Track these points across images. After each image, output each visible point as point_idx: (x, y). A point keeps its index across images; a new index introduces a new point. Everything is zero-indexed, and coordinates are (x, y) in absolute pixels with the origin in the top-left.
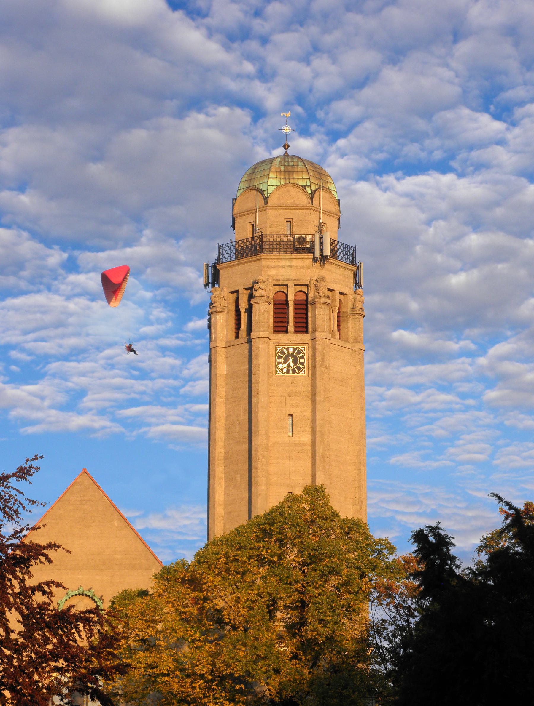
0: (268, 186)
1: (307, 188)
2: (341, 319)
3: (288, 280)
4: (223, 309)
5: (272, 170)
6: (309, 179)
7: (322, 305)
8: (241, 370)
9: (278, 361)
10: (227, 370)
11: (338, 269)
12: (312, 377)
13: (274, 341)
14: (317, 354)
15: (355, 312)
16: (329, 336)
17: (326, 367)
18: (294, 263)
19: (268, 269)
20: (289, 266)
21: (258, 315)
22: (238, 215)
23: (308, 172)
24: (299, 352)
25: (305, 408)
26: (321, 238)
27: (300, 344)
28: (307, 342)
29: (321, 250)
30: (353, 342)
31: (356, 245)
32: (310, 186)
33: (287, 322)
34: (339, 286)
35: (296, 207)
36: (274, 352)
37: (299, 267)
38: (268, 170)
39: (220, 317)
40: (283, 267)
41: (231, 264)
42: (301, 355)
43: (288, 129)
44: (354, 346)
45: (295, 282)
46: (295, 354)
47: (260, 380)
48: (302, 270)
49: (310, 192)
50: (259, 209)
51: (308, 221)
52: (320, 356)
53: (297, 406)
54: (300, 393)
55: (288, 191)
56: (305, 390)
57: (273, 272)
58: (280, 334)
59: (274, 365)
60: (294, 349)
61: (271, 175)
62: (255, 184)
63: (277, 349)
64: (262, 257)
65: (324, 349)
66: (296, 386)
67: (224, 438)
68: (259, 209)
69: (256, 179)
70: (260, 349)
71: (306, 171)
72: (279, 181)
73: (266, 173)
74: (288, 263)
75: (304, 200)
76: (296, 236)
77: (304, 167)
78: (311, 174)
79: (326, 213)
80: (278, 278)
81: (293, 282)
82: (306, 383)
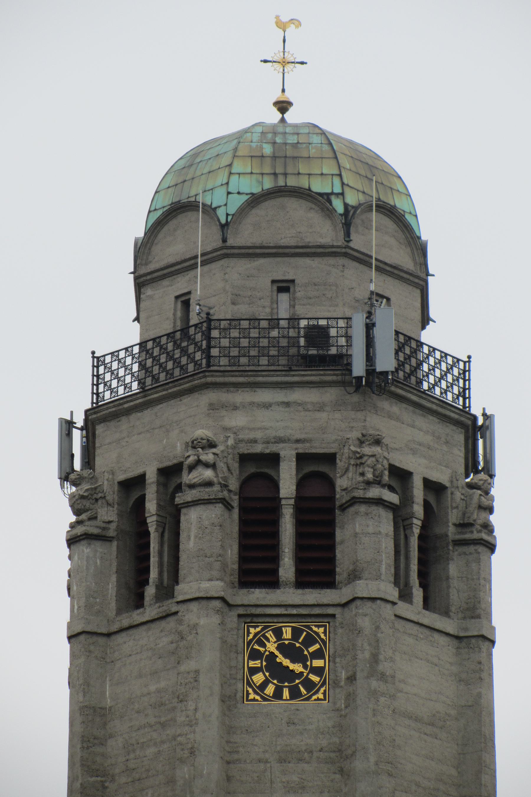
0: (229, 193)
1: (333, 198)
3: (280, 440)
4: (104, 529)
8: (149, 694)
9: (252, 664)
13: (241, 611)
15: (468, 536)
16: (393, 593)
17: (383, 677)
19: (224, 413)
20: (283, 403)
22: (149, 277)
23: (336, 158)
24: (310, 640)
26: (370, 327)
27: (313, 620)
28: (330, 611)
29: (370, 358)
30: (464, 618)
31: (469, 357)
32: (342, 194)
33: (276, 559)
34: (423, 461)
36: (241, 641)
37: (309, 407)
40: (267, 406)
41: (126, 406)
42: (316, 647)
44: (466, 629)
45: (299, 445)
46: (298, 645)
48: (318, 415)
50: (205, 258)
51: (337, 286)
54: (311, 752)
58: (257, 591)
59: (240, 676)
60: (296, 633)
62: (193, 193)
65: (378, 628)
67: (113, 526)
68: (205, 258)
71: (331, 155)
72: (258, 181)
74: (279, 396)
76: (303, 323)
79: (388, 268)
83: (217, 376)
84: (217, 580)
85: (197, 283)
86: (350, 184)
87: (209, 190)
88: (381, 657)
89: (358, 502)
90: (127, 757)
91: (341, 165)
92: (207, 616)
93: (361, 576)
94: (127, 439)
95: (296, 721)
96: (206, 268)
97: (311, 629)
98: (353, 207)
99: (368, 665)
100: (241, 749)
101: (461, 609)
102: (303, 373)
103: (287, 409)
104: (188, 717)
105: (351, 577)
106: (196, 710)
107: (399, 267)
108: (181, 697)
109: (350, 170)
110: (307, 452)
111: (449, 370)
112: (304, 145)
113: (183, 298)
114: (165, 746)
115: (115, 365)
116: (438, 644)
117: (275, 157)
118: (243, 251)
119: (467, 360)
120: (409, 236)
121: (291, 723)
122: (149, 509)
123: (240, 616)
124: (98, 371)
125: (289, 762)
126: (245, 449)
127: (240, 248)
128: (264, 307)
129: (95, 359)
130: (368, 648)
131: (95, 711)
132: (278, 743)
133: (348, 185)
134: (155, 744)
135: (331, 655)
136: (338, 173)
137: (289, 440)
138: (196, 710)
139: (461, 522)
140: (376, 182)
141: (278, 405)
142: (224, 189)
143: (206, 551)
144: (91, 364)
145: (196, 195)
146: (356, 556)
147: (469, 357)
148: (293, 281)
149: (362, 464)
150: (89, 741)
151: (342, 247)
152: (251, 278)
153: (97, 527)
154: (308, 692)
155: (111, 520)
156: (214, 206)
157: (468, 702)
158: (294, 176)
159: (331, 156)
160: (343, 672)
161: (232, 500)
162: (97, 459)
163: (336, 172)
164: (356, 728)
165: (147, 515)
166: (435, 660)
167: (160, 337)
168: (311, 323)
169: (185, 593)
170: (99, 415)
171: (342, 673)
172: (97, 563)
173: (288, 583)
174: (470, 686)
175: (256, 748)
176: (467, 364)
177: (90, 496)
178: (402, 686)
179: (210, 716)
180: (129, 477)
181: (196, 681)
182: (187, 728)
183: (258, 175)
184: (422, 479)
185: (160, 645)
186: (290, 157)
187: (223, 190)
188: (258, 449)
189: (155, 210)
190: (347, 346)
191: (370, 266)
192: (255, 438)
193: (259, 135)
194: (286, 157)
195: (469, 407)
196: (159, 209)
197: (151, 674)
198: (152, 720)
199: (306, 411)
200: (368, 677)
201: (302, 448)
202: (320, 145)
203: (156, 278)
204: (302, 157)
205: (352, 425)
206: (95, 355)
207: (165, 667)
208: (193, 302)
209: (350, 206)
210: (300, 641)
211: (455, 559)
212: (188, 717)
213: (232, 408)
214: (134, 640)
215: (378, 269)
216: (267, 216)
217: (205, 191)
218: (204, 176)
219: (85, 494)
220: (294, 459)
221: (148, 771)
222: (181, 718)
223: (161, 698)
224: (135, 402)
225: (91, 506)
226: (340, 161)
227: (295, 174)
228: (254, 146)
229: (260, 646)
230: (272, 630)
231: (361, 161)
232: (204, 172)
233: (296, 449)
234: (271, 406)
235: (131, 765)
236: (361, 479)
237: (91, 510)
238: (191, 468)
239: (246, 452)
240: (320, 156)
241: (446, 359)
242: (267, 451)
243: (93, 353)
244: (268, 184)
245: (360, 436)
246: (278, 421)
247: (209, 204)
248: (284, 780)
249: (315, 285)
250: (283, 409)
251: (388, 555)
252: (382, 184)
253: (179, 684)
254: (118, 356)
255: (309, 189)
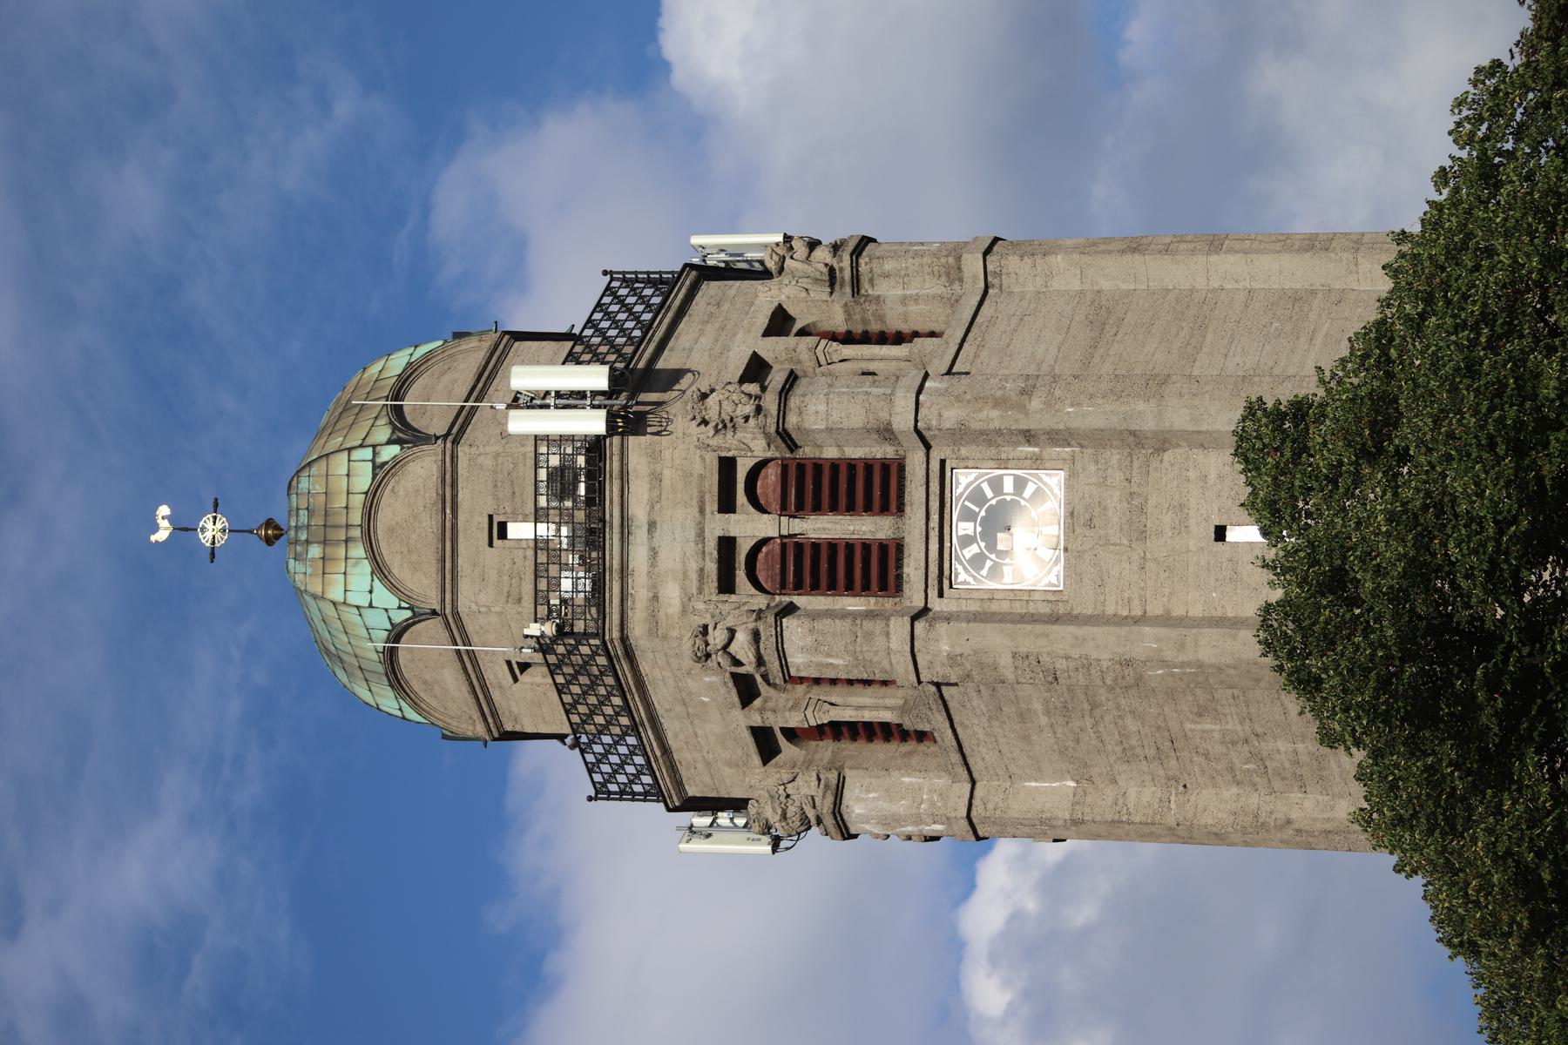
0: (371, 606)
1: (379, 460)
2: (875, 327)
3: (701, 535)
4: (827, 786)
5: (319, 590)
6: (350, 450)
7: (794, 402)
10: (1059, 775)
11: (677, 338)
12: (1069, 445)
13: (933, 593)
14: (976, 425)
15: (847, 275)
18: (639, 511)
19: (661, 615)
20: (649, 531)
21: (829, 655)
22: (490, 720)
23: (327, 455)
25: (1192, 474)
28: (935, 466)
31: (605, 273)
32: (374, 446)
35: (448, 500)
38: (321, 604)
39: (858, 799)
40: (654, 553)
41: (658, 753)
43: (210, 525)
44: (975, 277)
45: (708, 510)
47: (1075, 653)
48: (666, 482)
49: (395, 450)
52: (982, 415)
53: (1181, 506)
55: (391, 530)
56: (1119, 476)
57: (672, 594)
60: (968, 516)
61: (336, 593)
62: (374, 656)
63: (965, 583)
64: (616, 635)
66: (1105, 508)
67: (1320, 798)
69: (358, 652)
70: (958, 651)
71: (323, 462)
72: (355, 565)
73: (330, 611)
74: (640, 537)
75: (424, 467)
77: (314, 470)
78: (336, 441)
80: (694, 576)
81: (708, 515)
82: (1093, 468)
83: (611, 624)
84: (888, 625)
85: (494, 651)
86: (363, 437)
87: (369, 634)
88: (999, 394)
89: (783, 425)
90: (1142, 758)
91: (337, 449)
92: (938, 641)
93: (885, 422)
94: (705, 753)
95: (1087, 517)
96: (474, 638)
97: (962, 494)
98: (393, 432)
99: (1010, 413)
100: (1126, 595)
101: (947, 284)
102: (607, 503)
103: (658, 526)
104: (1077, 670)
105: (887, 436)
106: (1067, 658)
107: (481, 369)
108: (1050, 679)
109: (345, 436)
110: (716, 498)
111: (620, 301)
112: (311, 500)
113: (517, 671)
114: (1123, 702)
115: (606, 768)
116: (992, 317)
117: (325, 541)
118: (448, 586)
119: (609, 276)
120: (441, 356)
121: (1090, 524)
122: (798, 722)
123: (941, 595)
124: (615, 793)
125: (1145, 526)
126: (712, 583)
127: (443, 591)
128: (525, 558)
129: (599, 796)
130: (985, 412)
131: (1078, 803)
132: (1118, 541)
133: (364, 439)
134: (1120, 717)
135: (997, 466)
136: (346, 453)
137: (700, 523)
138: (1067, 658)
139: (828, 284)
140: (363, 405)
141: (653, 537)
142: (365, 612)
143: (848, 641)
144: (606, 802)
145: (377, 652)
146: (858, 429)
147: (605, 273)
148: (491, 517)
149: (732, 420)
150: (1119, 812)
151: (445, 448)
152: (486, 576)
153: (824, 797)
154: (979, 486)
155: (815, 777)
156: (389, 627)
157: (1075, 275)
158: (350, 515)
159: (325, 463)
160: (1020, 449)
161: (781, 602)
162: (733, 795)
163: (345, 454)
164: (1097, 430)
165: (806, 726)
166: (1015, 320)
167: (563, 704)
168: (543, 491)
169: (906, 671)
170: (672, 792)
171: (1021, 452)
172: (874, 798)
173: (896, 526)
174: (1054, 272)
175: (1124, 574)
176: (614, 276)
177: (782, 806)
178: (1045, 367)
179: (1076, 638)
180: (757, 751)
181: (1027, 657)
182: (1093, 671)
183: (349, 564)
184: (764, 338)
185: (984, 709)
186: (325, 520)
187: (367, 613)
188: (712, 567)
189: (400, 709)
190: (573, 441)
191: (474, 410)
192: (697, 572)
193: (297, 562)
194: (325, 526)
195: (672, 273)
196: (399, 704)
197: (1024, 723)
198: (1089, 722)
199: (661, 499)
200: (1027, 414)
201: (712, 504)
202: (311, 479)
203: (491, 710)
204: (326, 503)
205: (681, 435)
206: (593, 796)
207: (1012, 702)
208: (520, 657)
209: (391, 436)
210: (977, 510)
211: (878, 293)
212: (1077, 670)
213: (656, 603)
214: (978, 746)
215: (479, 399)
216: (402, 552)
217: (370, 639)
218: (351, 641)
219: (780, 813)
220: (727, 516)
221: (1158, 728)
222: (1081, 678)
223: (1056, 708)
224: (653, 741)
225: (795, 804)
226: (332, 450)
227: (347, 513)
228: (311, 569)
229: (990, 568)
230: (961, 549)
231: (337, 422)
232: (347, 640)
233: (712, 513)
234: (654, 549)
235: (1151, 752)
236: (752, 421)
237: (801, 804)
238: (737, 662)
239: (716, 584)
240: (324, 478)
241: (604, 304)
242: (715, 553)
243: (590, 799)
244: (358, 551)
245: (694, 423)
246: (675, 539)
247: (387, 633)
248: (1170, 534)
249: (496, 486)
250: (658, 531)
251: (859, 385)
252: (368, 393)
253: (1032, 681)
254: (593, 764)
255: (366, 493)
